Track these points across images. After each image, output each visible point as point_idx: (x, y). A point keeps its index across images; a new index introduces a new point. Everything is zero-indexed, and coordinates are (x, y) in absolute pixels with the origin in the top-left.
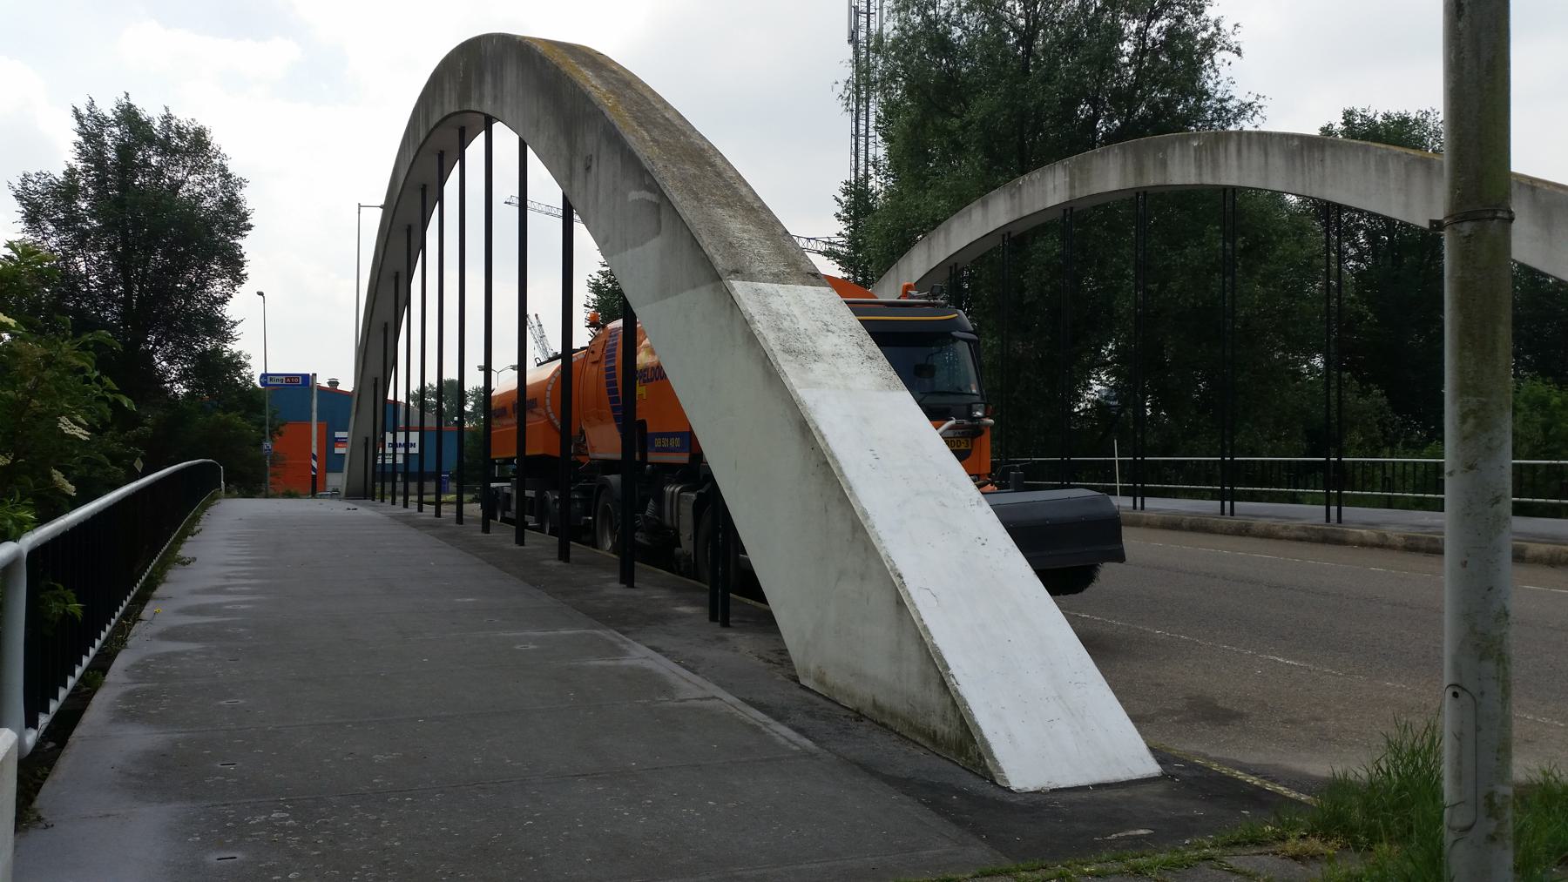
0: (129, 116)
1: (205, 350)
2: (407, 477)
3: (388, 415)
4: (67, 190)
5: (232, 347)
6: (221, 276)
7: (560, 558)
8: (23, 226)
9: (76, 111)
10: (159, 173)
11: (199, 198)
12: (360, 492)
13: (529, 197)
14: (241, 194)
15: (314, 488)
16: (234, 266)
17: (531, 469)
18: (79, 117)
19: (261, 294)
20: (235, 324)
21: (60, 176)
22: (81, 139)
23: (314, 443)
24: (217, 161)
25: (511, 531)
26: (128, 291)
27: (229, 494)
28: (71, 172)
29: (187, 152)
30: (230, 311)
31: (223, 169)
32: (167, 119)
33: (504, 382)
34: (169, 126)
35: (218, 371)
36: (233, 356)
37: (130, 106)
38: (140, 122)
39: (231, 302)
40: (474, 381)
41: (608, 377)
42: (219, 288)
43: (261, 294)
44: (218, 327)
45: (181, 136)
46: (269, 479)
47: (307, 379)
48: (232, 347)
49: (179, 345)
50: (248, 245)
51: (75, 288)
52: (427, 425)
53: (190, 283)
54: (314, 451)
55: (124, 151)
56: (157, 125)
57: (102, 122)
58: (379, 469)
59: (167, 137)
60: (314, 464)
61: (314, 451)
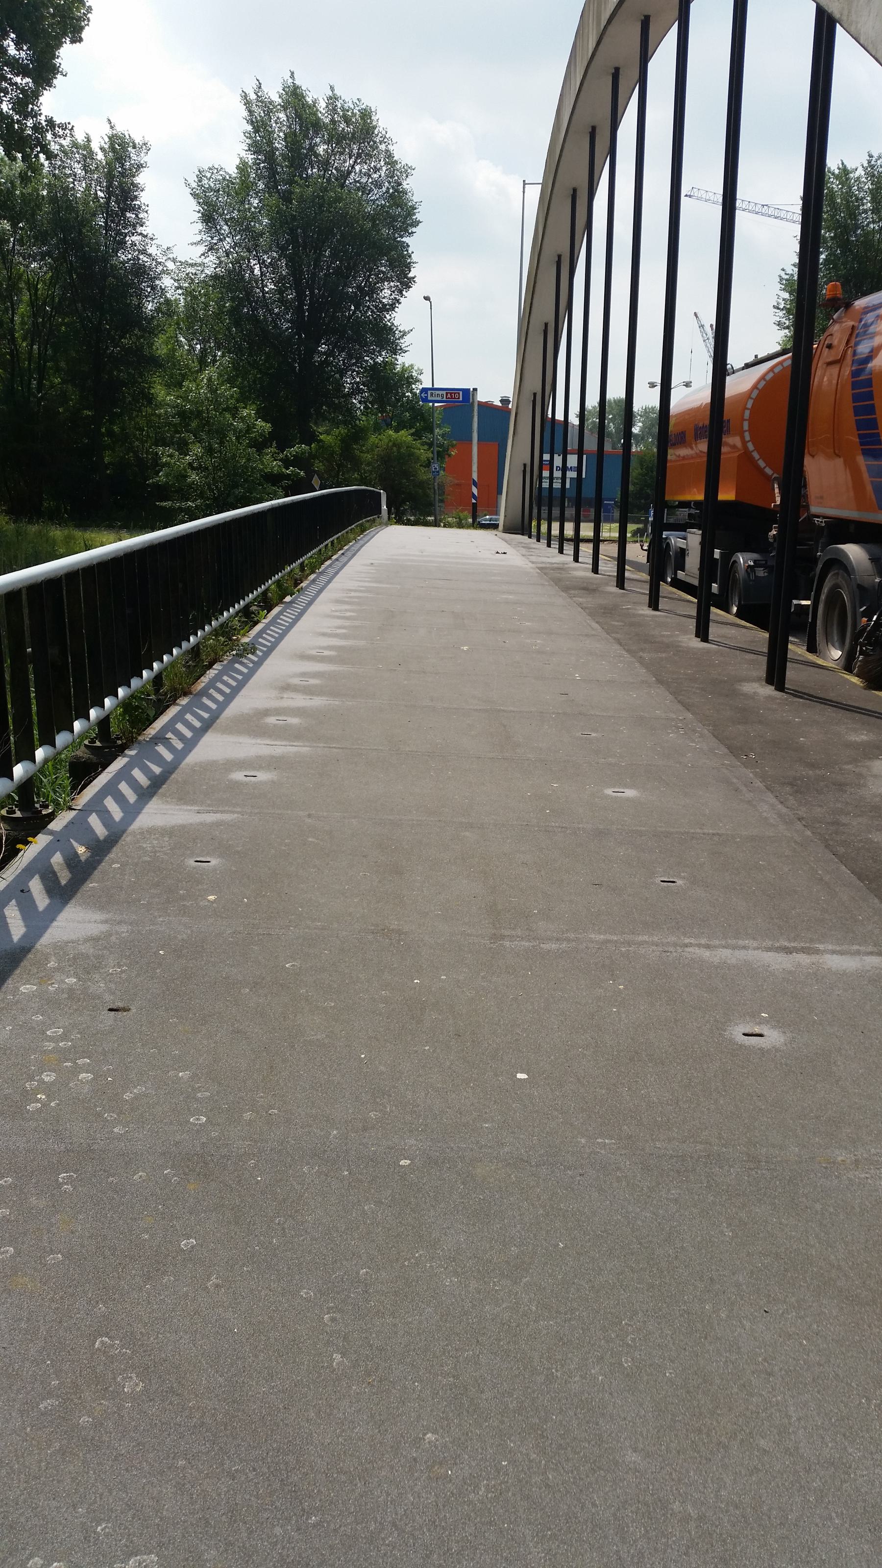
0: (294, 96)
1: (376, 363)
2: (578, 503)
3: (552, 434)
4: (241, 187)
5: (403, 360)
6: (389, 280)
7: (770, 680)
8: (200, 226)
9: (245, 96)
10: (325, 164)
11: (363, 188)
12: (520, 527)
13: (718, 210)
14: (407, 184)
15: (476, 516)
16: (401, 271)
17: (724, 524)
18: (248, 103)
19: (427, 298)
20: (404, 334)
21: (233, 171)
22: (249, 128)
23: (475, 468)
24: (383, 147)
25: (689, 604)
26: (300, 296)
27: (390, 522)
28: (243, 168)
29: (353, 138)
30: (400, 318)
31: (389, 155)
32: (333, 99)
33: (692, 390)
34: (334, 110)
35: (389, 385)
36: (404, 370)
37: (296, 88)
38: (305, 105)
39: (400, 309)
40: (646, 399)
41: (856, 398)
42: (386, 292)
43: (427, 298)
44: (387, 338)
45: (347, 121)
46: (437, 504)
47: (468, 394)
48: (403, 360)
49: (350, 356)
50: (416, 244)
51: (249, 293)
52: (586, 447)
53: (359, 287)
54: (475, 476)
55: (292, 140)
56: (322, 105)
57: (268, 108)
58: (545, 494)
59: (333, 121)
60: (475, 490)
61: (475, 476)
